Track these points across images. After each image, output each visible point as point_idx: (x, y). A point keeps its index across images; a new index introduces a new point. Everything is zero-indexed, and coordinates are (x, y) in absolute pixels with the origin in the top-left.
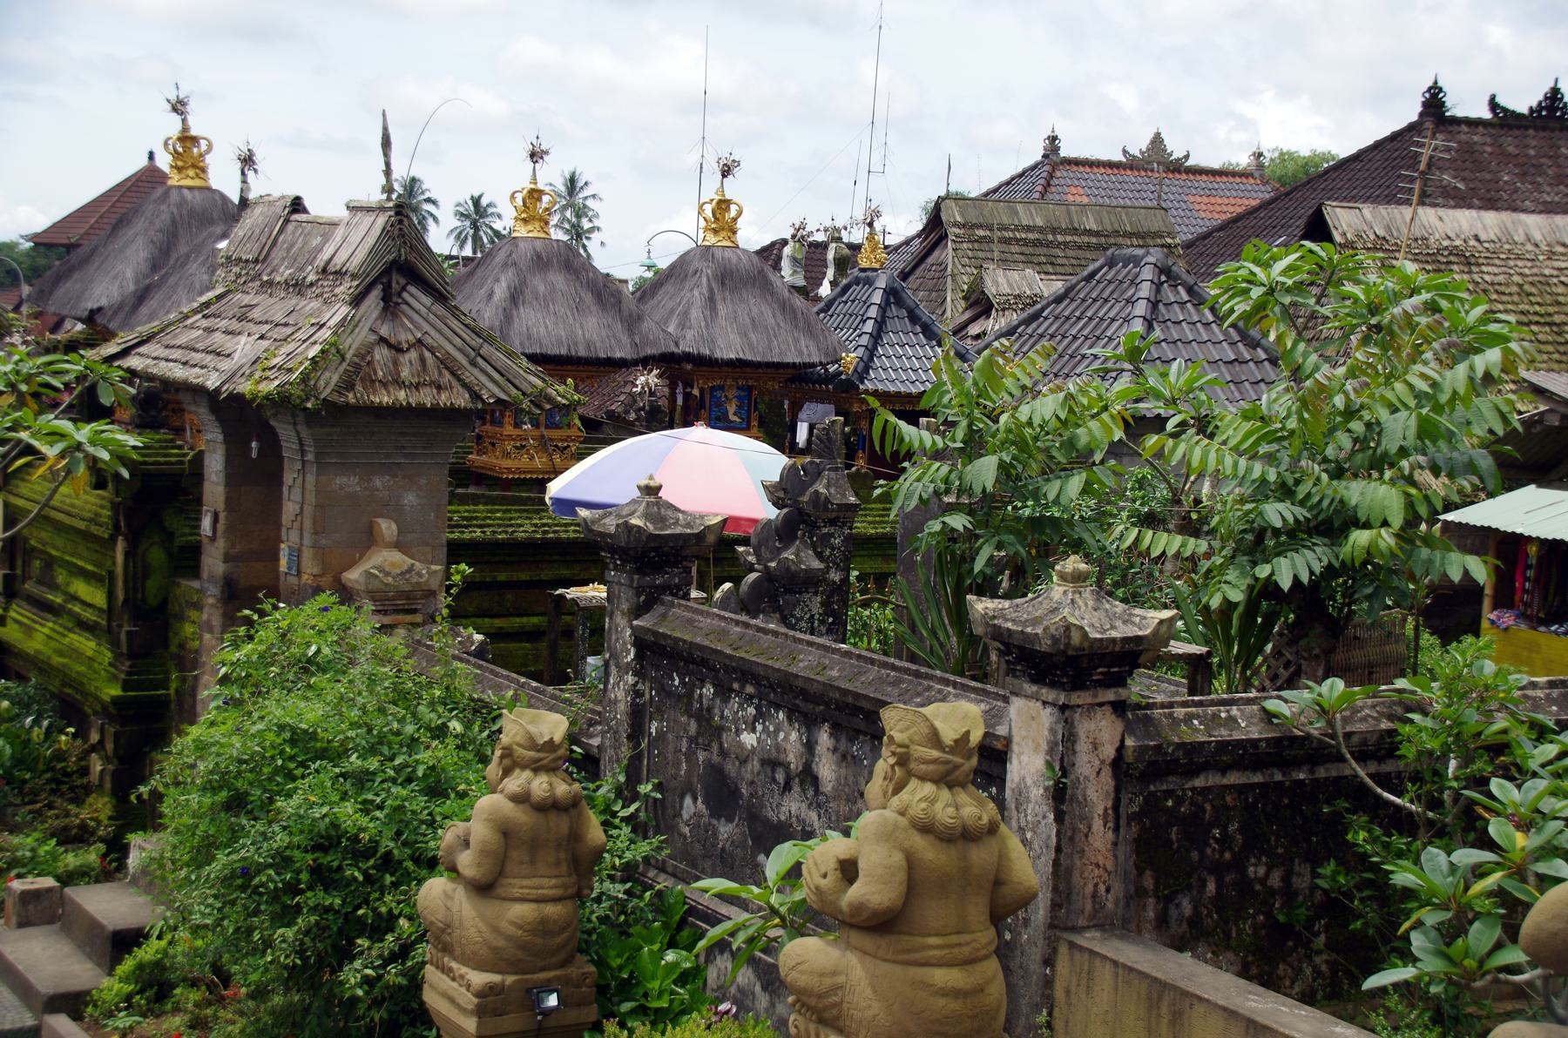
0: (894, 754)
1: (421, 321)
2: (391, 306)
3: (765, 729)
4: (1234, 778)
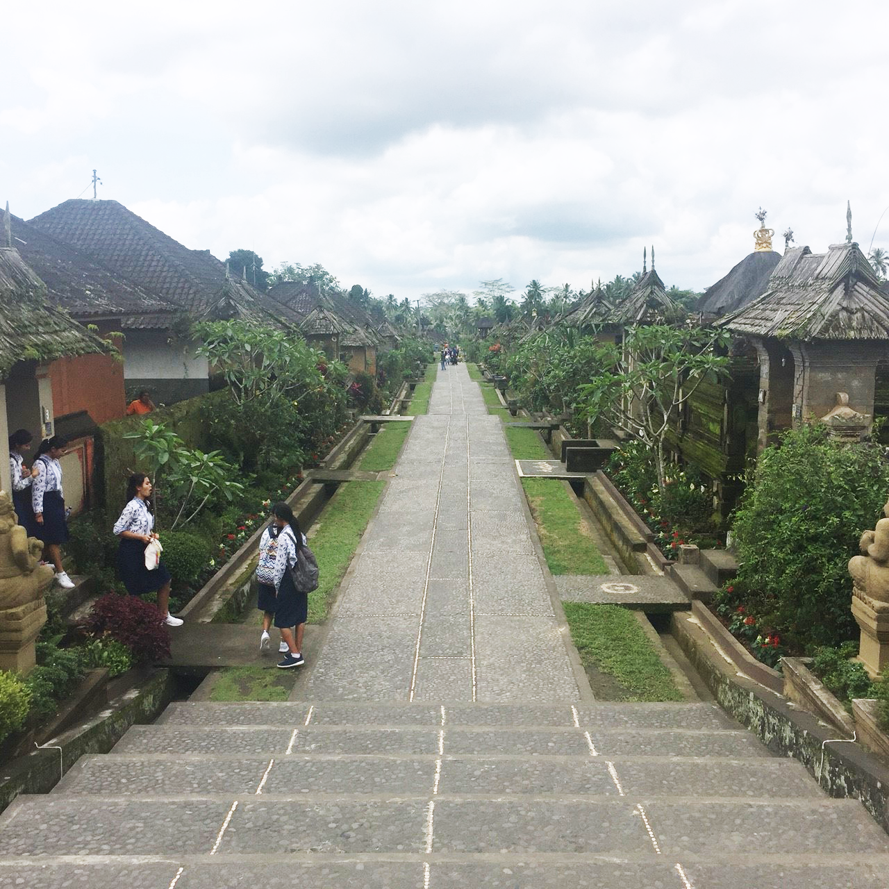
1: (864, 299)
2: (848, 293)
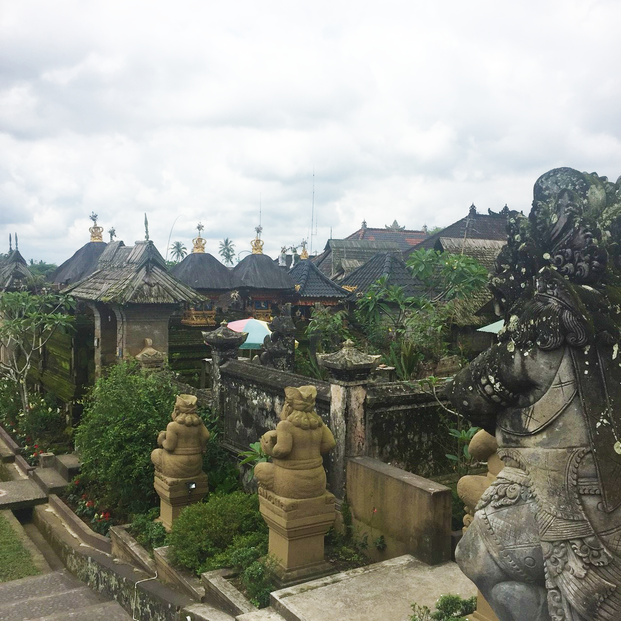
0: (288, 402)
1: (158, 277)
2: (149, 273)
3: (260, 398)
4: (402, 407)
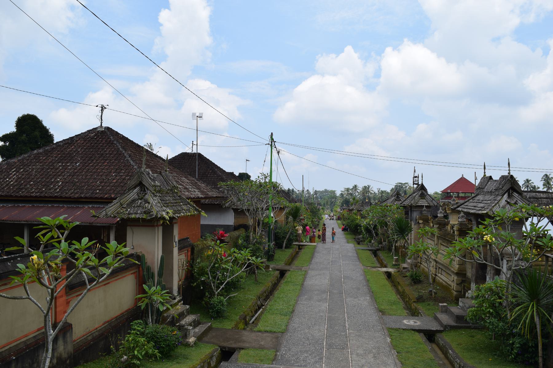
2: (510, 196)
